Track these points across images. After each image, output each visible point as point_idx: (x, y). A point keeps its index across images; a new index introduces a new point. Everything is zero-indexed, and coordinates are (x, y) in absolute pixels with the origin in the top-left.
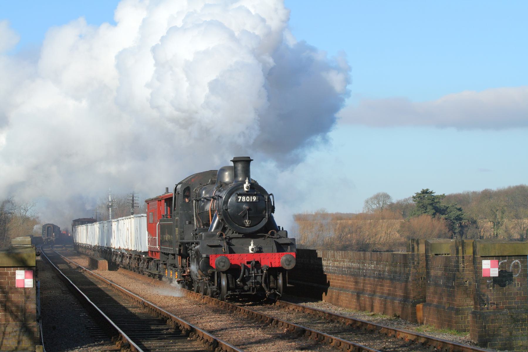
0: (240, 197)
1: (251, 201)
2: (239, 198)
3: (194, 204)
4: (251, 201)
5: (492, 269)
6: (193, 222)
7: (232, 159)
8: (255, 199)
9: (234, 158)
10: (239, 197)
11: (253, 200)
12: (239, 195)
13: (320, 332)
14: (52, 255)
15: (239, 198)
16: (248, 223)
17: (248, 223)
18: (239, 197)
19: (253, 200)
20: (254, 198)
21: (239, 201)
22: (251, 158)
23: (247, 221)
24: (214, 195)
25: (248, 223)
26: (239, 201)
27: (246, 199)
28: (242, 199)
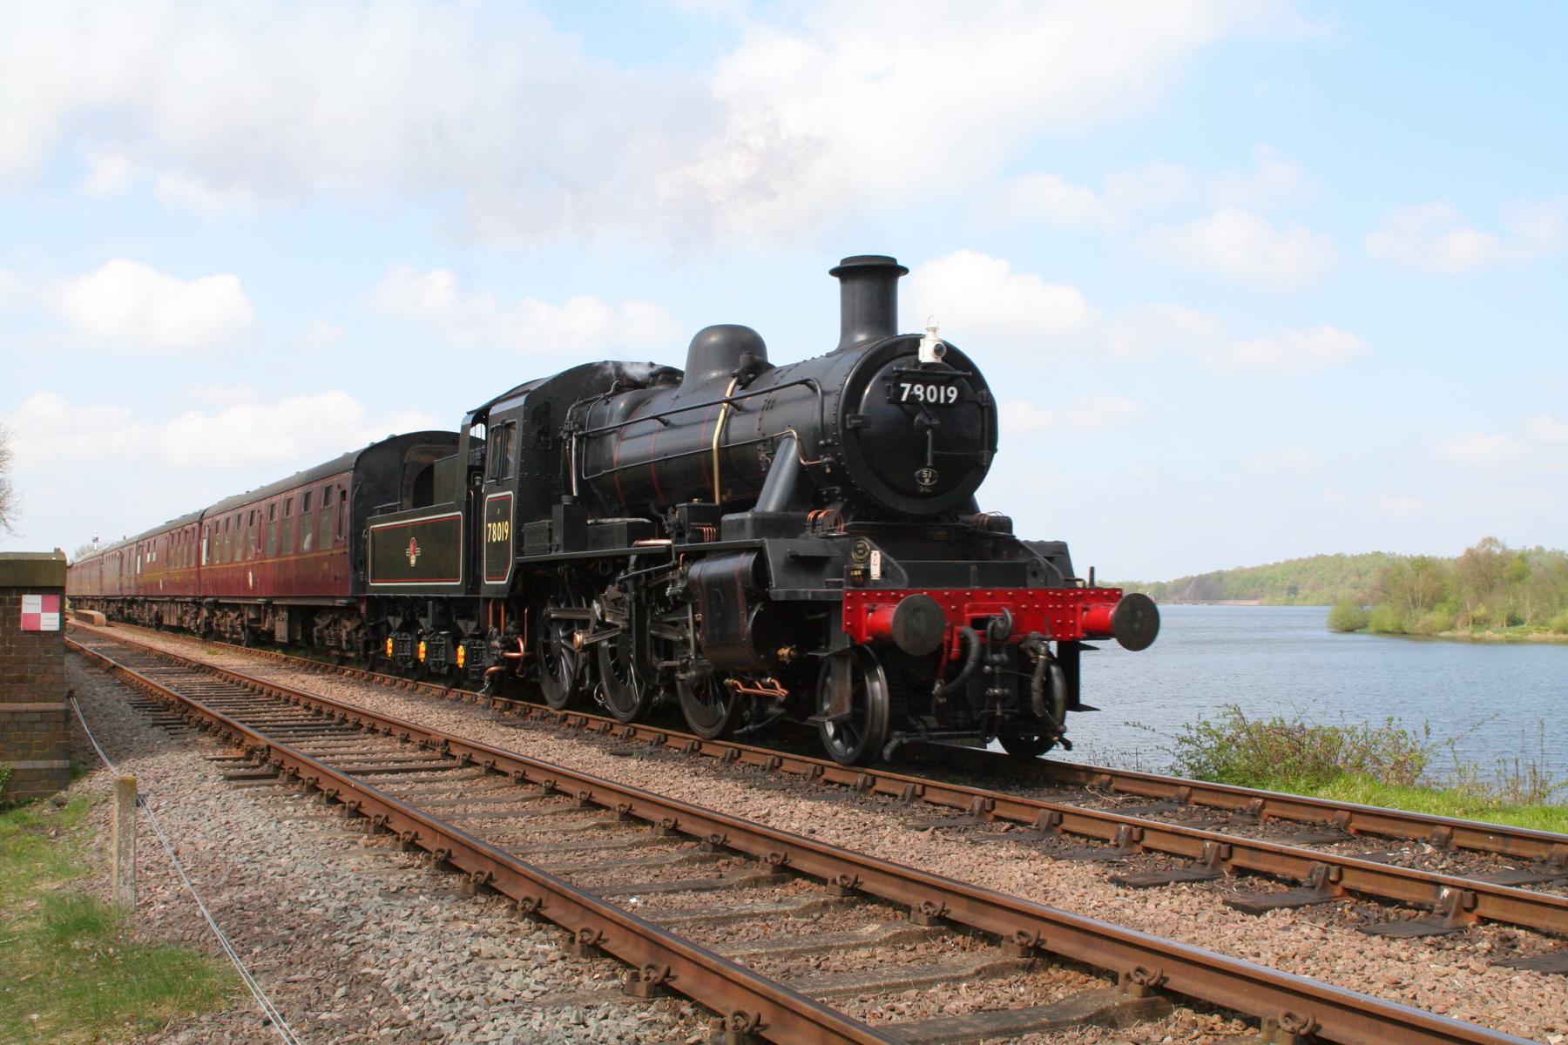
0: (908, 386)
1: (942, 401)
2: (904, 388)
3: (240, 602)
4: (942, 401)
5: (44, 616)
6: (984, 392)
7: (837, 264)
8: (954, 397)
9: (844, 261)
10: (903, 385)
11: (947, 398)
12: (902, 376)
13: (1349, 991)
14: (556, 884)
15: (904, 388)
16: (930, 482)
17: (927, 481)
18: (903, 385)
19: (947, 398)
20: (952, 392)
21: (904, 398)
22: (900, 263)
23: (924, 471)
24: (731, 395)
25: (927, 481)
26: (904, 398)
27: (925, 393)
28: (912, 389)
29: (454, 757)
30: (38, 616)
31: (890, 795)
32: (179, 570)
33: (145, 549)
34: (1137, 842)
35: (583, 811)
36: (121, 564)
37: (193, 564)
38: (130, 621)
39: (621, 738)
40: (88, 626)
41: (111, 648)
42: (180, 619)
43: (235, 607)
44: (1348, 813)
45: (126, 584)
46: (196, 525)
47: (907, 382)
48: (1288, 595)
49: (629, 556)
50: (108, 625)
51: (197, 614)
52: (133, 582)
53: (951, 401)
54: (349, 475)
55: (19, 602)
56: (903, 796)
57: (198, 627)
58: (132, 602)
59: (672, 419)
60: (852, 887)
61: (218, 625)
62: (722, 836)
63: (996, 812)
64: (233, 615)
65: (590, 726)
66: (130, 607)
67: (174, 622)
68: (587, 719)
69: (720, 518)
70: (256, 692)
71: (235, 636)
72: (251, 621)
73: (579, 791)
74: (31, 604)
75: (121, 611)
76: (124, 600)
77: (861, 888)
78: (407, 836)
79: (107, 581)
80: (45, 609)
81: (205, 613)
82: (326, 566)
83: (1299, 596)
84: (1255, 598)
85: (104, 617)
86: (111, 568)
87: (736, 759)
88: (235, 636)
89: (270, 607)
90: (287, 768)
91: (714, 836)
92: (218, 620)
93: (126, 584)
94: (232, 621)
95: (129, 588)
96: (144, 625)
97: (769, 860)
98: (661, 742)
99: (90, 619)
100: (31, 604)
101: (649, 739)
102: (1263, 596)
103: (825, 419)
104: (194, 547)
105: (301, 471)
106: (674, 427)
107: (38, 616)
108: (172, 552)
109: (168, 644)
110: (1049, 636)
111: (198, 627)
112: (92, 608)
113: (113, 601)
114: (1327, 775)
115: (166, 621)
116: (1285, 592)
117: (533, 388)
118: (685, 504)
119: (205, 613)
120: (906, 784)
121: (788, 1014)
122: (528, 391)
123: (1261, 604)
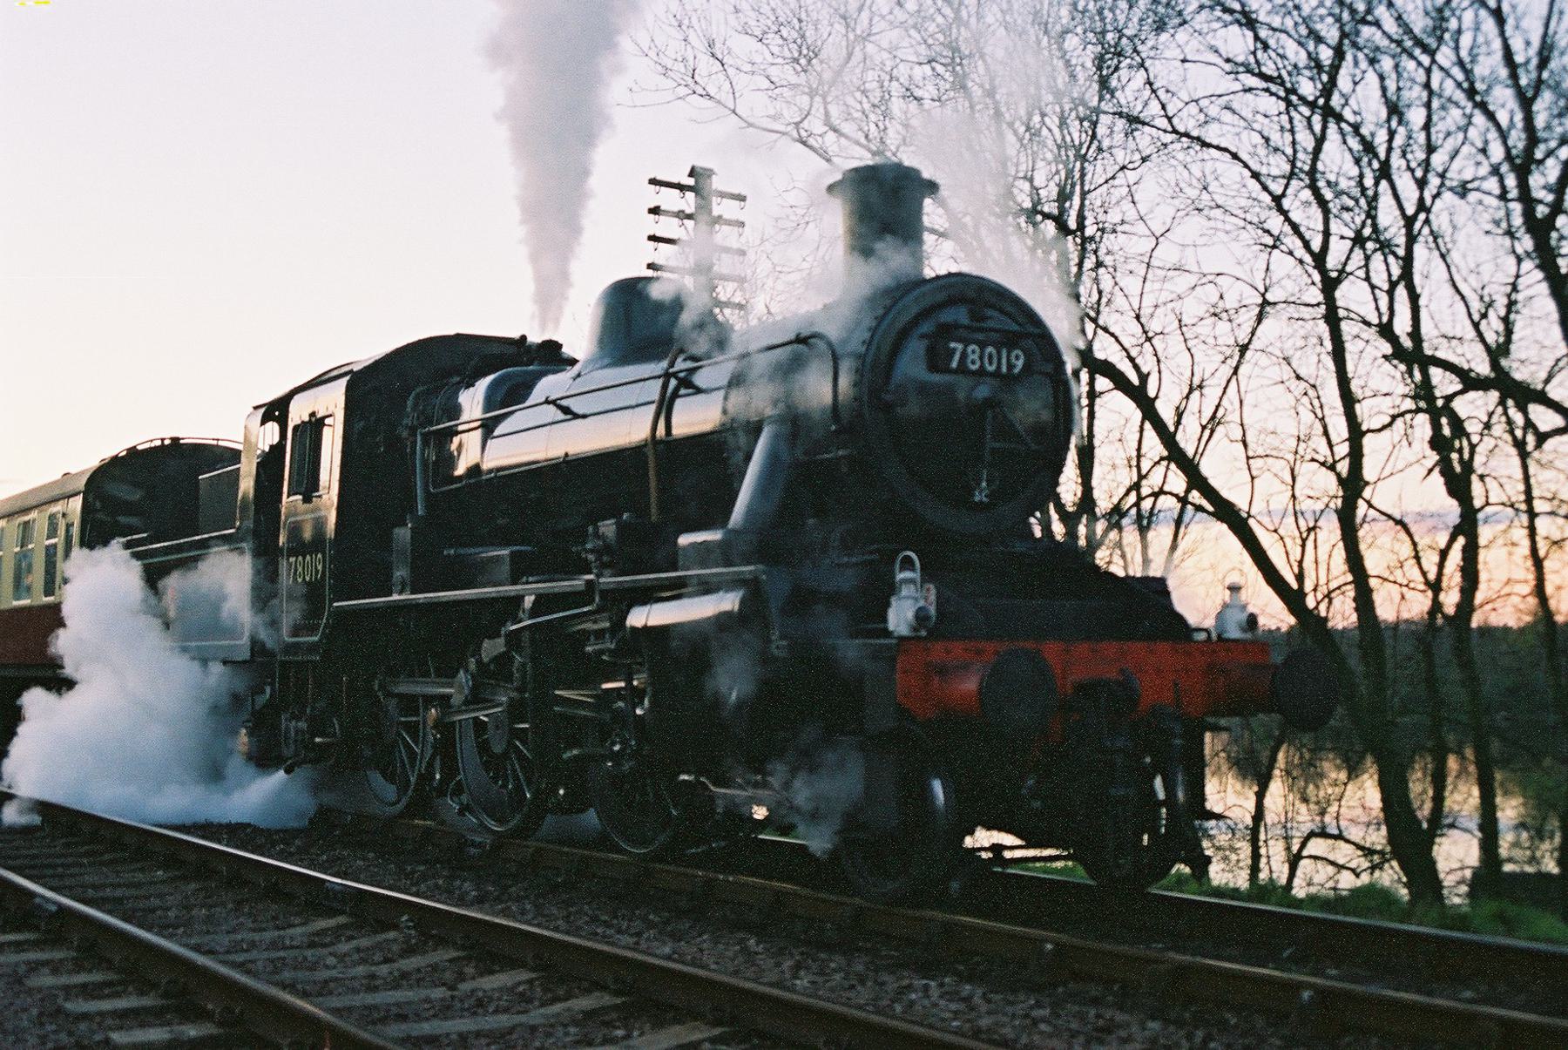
1: (1004, 369)
2: (954, 350)
4: (1004, 369)
8: (1020, 363)
10: (953, 345)
11: (1010, 366)
15: (954, 350)
18: (953, 345)
19: (1010, 366)
27: (981, 358)
47: (959, 340)
49: (523, 597)
53: (1016, 371)
54: (76, 504)
59: (576, 405)
65: (1281, 872)
69: (675, 543)
103: (840, 398)
106: (576, 416)
110: (1328, 745)
114: (1323, 992)
117: (356, 368)
118: (505, 552)
122: (351, 372)
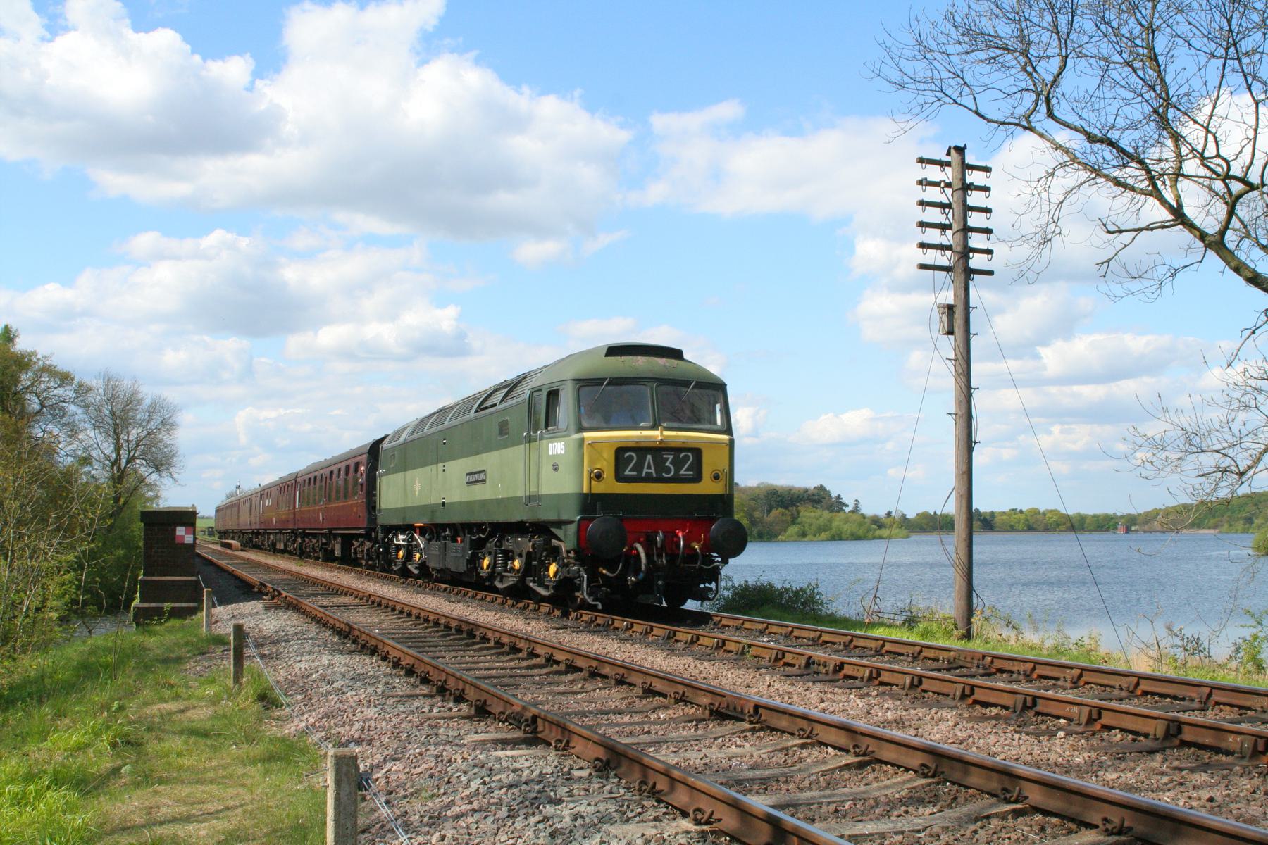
5: (186, 536)
29: (538, 656)
30: (183, 537)
31: (943, 695)
32: (284, 510)
33: (265, 496)
34: (1175, 736)
35: (647, 697)
36: (251, 506)
37: (291, 508)
38: (257, 547)
39: (641, 634)
40: (229, 551)
41: (239, 563)
42: (286, 546)
43: (314, 535)
44: (1209, 689)
45: (253, 521)
46: (293, 482)
48: (1245, 524)
50: (242, 550)
51: (295, 541)
52: (258, 519)
54: (366, 456)
55: (175, 530)
56: (1014, 708)
57: (295, 549)
58: (257, 533)
60: (621, 680)
61: (306, 548)
62: (649, 683)
63: (785, 660)
64: (314, 541)
66: (257, 538)
67: (282, 547)
68: (596, 617)
70: (376, 605)
71: (370, 563)
72: (323, 544)
73: (641, 681)
74: (180, 531)
75: (251, 540)
76: (253, 533)
77: (654, 689)
78: (439, 683)
79: (242, 518)
80: (183, 537)
81: (299, 540)
82: (355, 509)
83: (1254, 525)
84: (1215, 527)
85: (239, 544)
86: (245, 508)
87: (1095, 720)
88: (370, 563)
89: (331, 535)
90: (391, 657)
91: (711, 704)
92: (355, 549)
93: (253, 521)
94: (313, 545)
95: (255, 523)
96: (266, 550)
97: (673, 696)
98: (671, 636)
99: (229, 546)
100: (180, 531)
101: (640, 630)
102: (1222, 526)
104: (292, 496)
105: (328, 458)
107: (183, 537)
108: (280, 499)
109: (453, 605)
111: (295, 549)
112: (233, 539)
113: (246, 533)
115: (278, 547)
116: (1241, 522)
119: (299, 540)
120: (771, 651)
121: (695, 792)
123: (1220, 532)
